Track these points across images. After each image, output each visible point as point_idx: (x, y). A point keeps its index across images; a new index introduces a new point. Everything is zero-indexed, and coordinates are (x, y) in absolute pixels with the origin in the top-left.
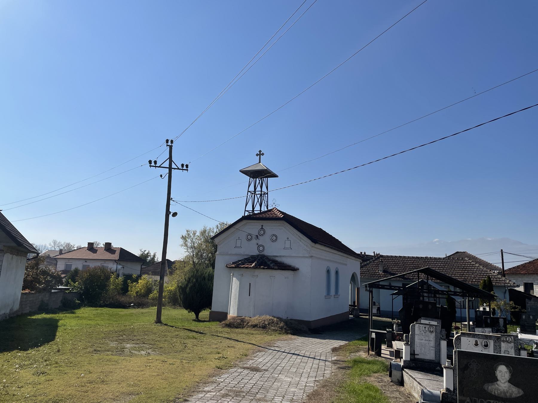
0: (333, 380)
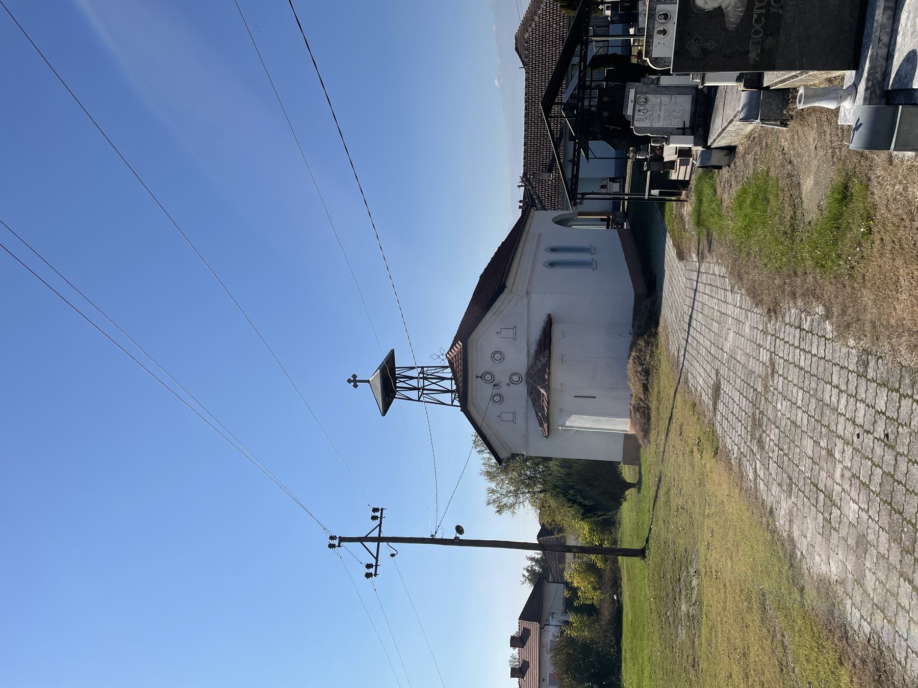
0: (730, 262)
